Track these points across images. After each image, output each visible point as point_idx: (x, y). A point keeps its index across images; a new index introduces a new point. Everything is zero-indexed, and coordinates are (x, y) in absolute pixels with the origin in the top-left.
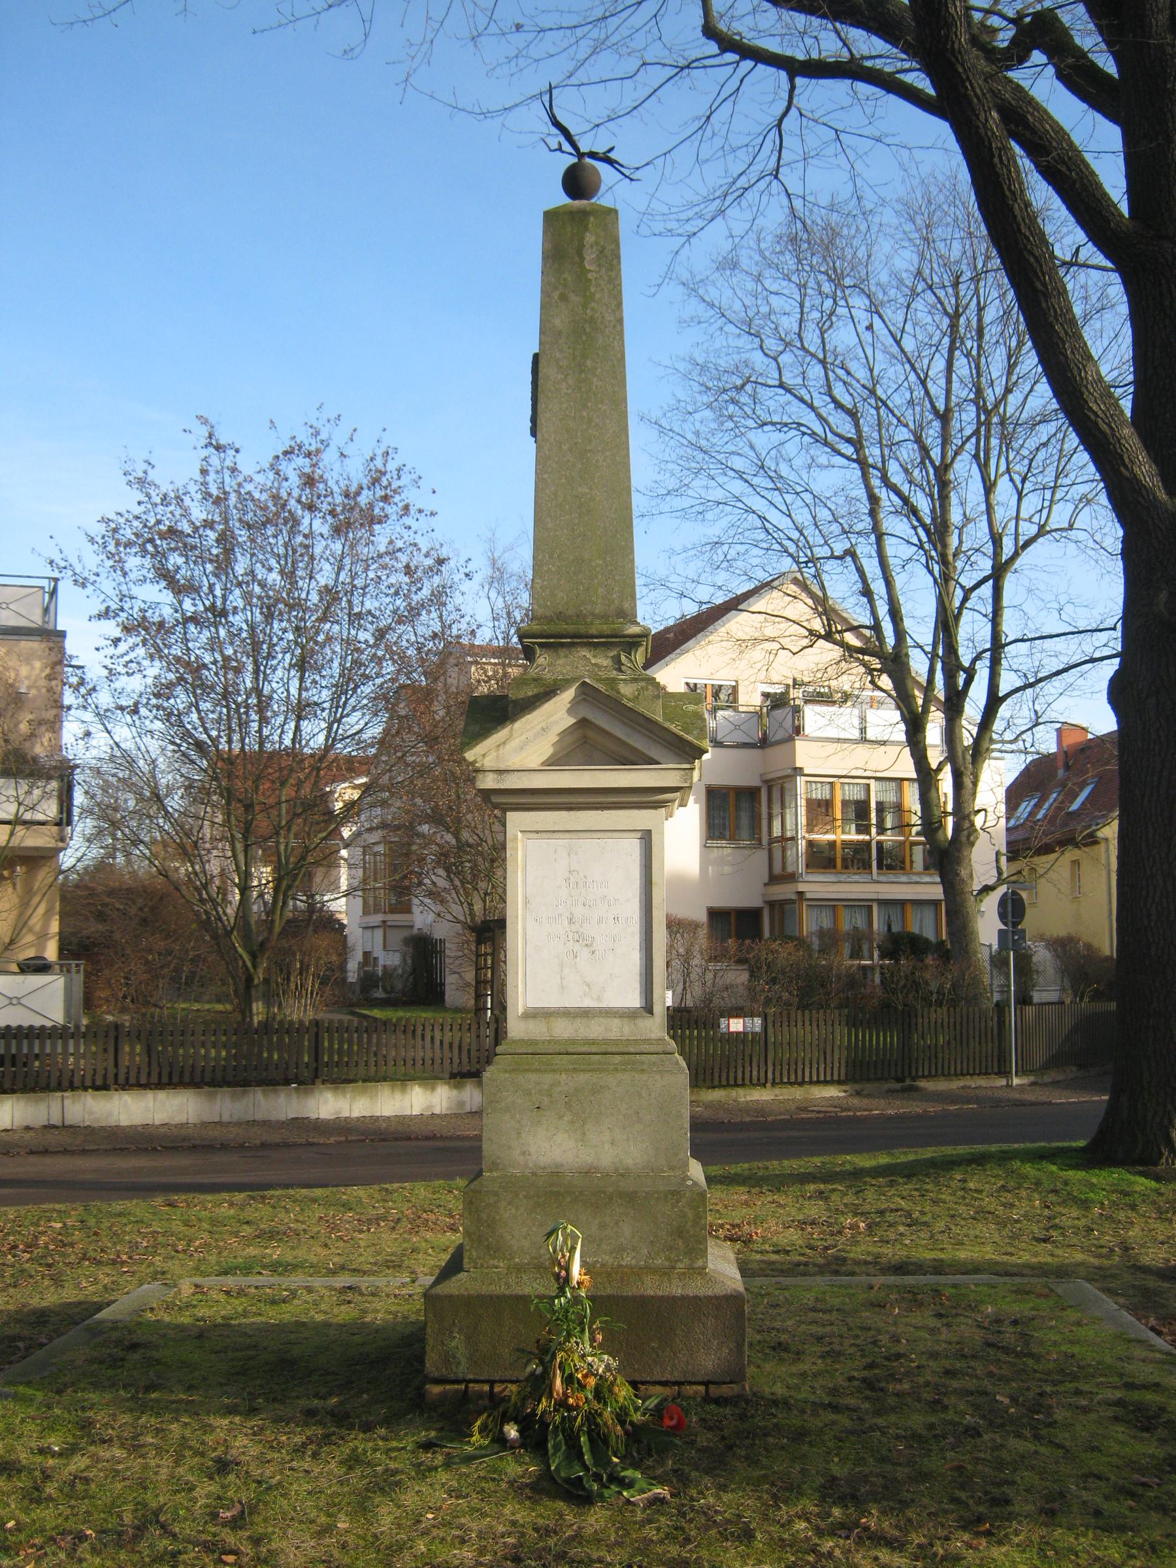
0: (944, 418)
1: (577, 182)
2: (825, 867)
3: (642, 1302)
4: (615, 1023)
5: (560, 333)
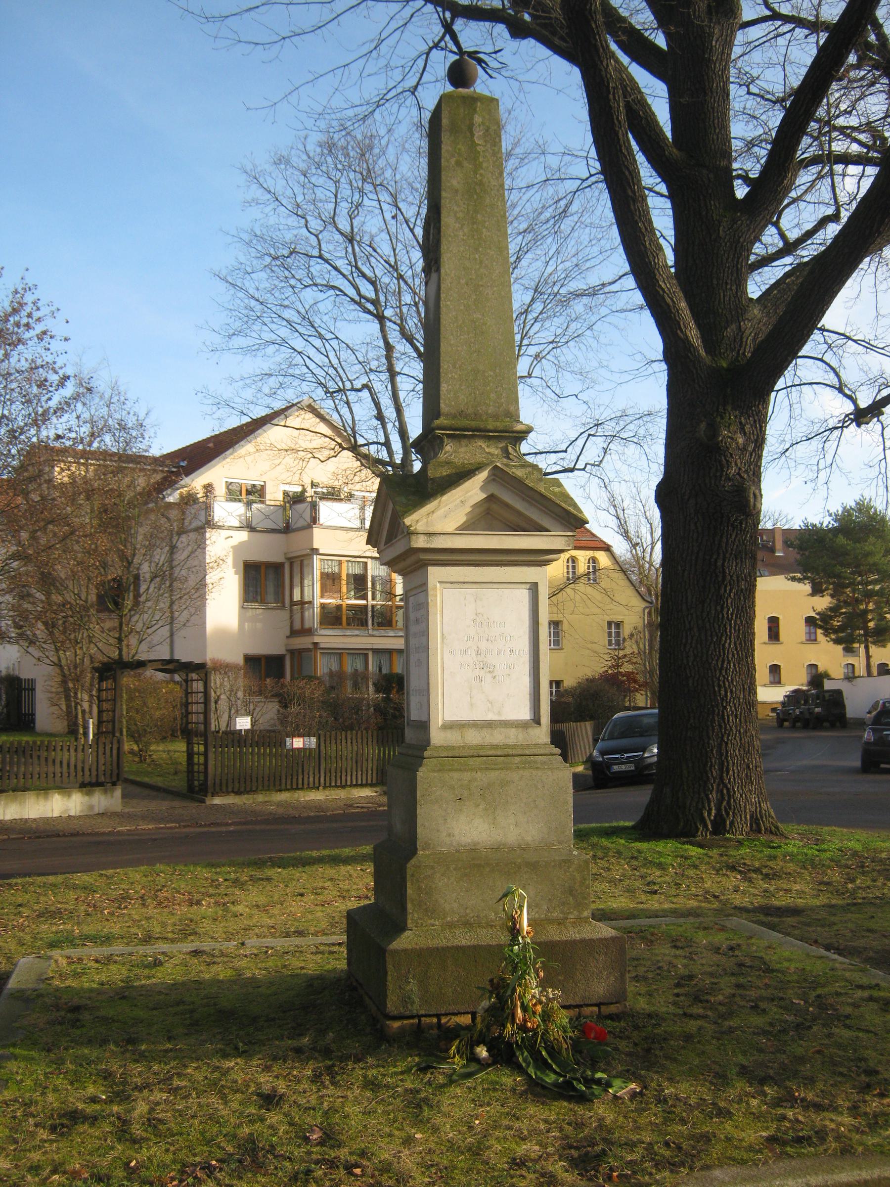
2: (333, 624)
4: (512, 732)
5: (457, 191)
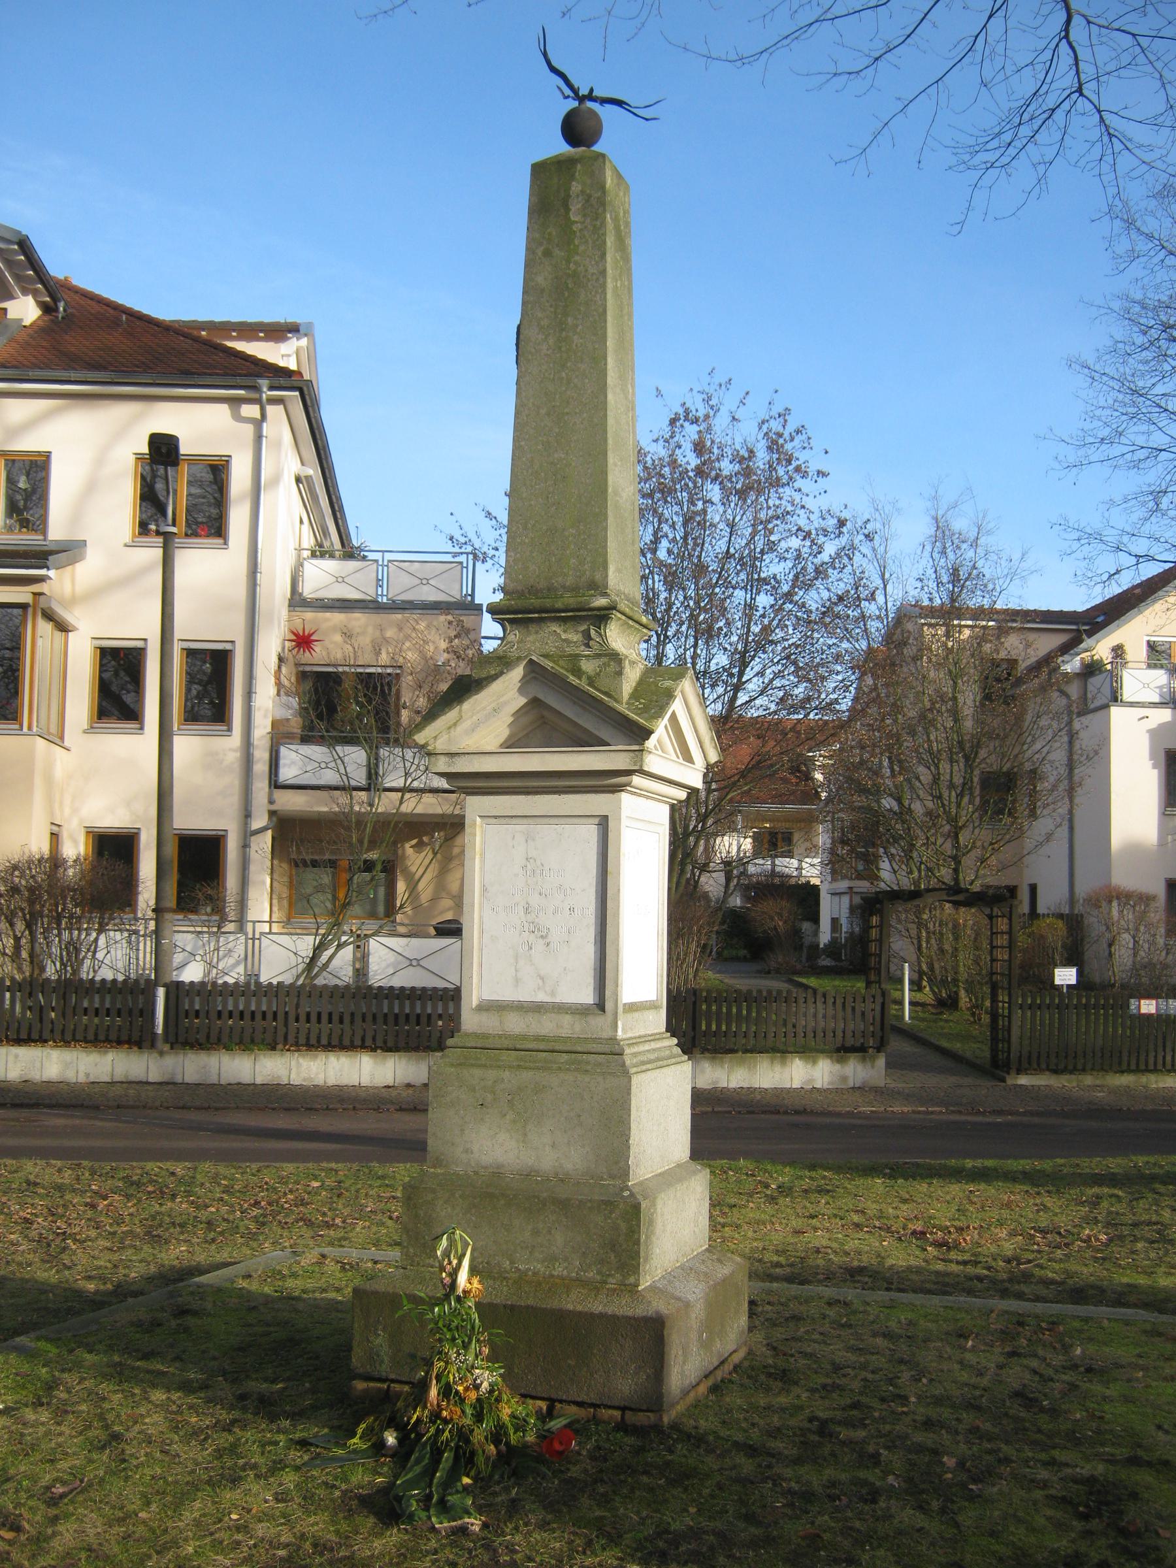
1: (578, 130)
3: (560, 1318)
5: (543, 291)
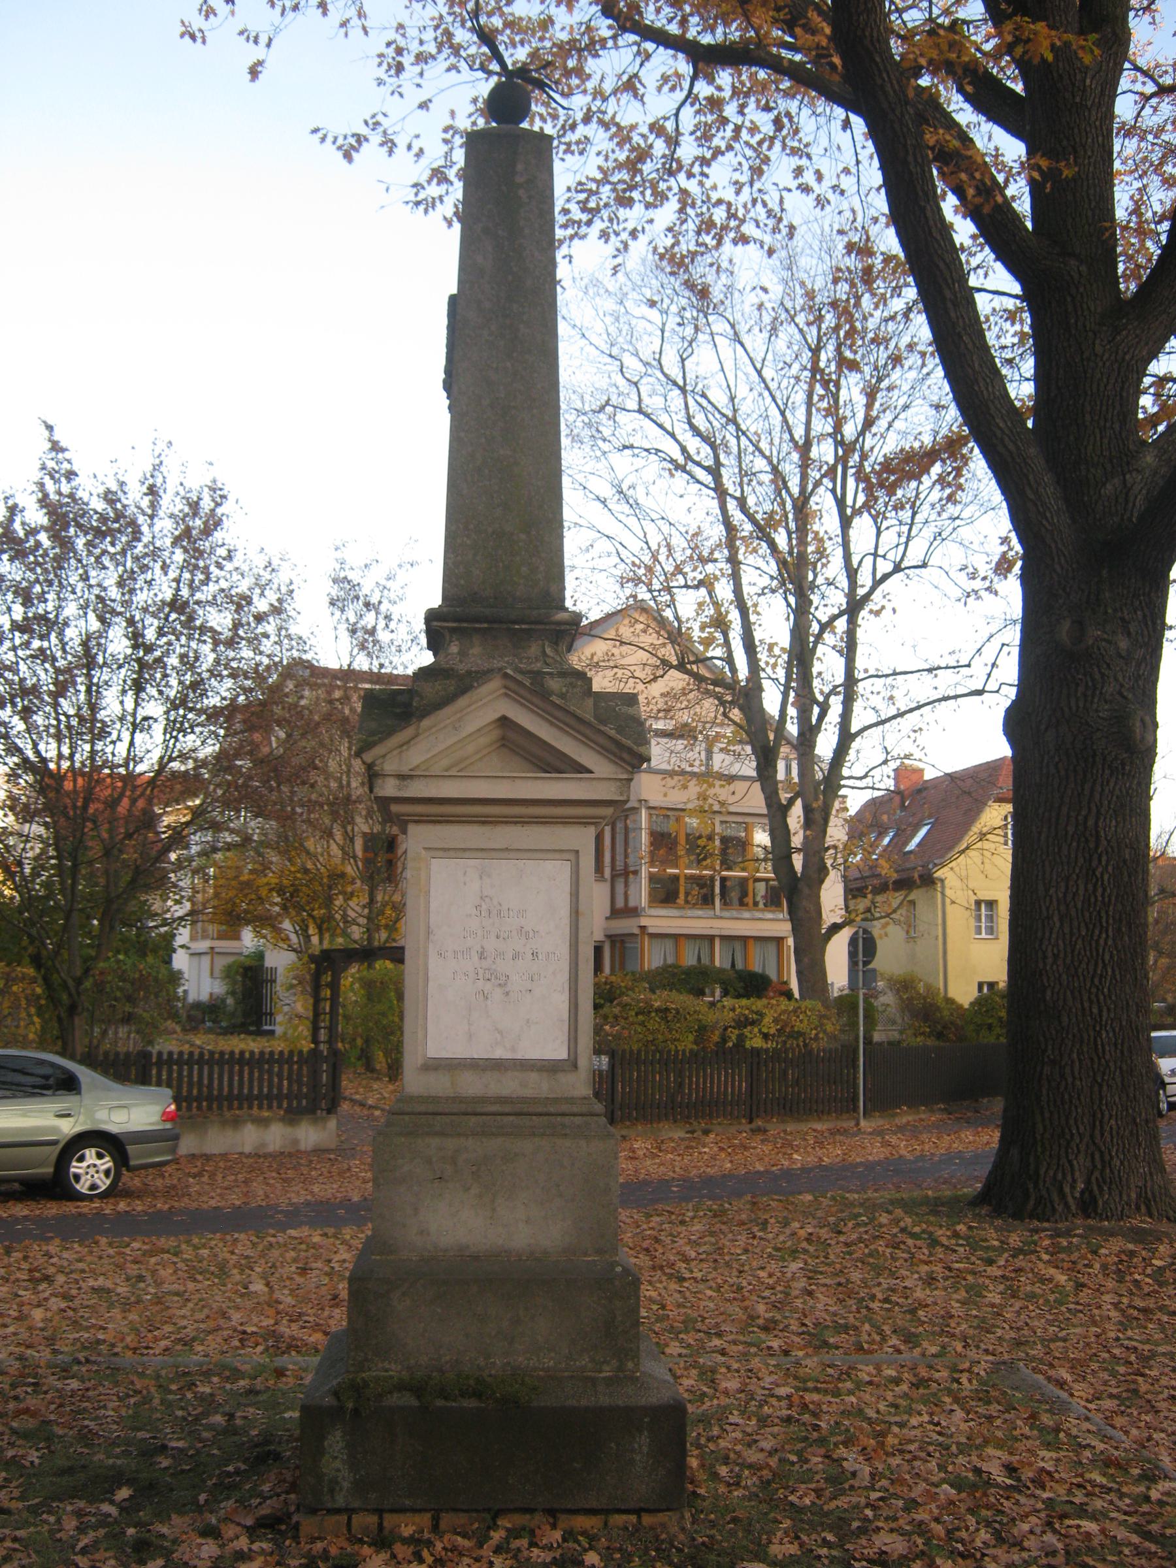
0: (804, 449)
